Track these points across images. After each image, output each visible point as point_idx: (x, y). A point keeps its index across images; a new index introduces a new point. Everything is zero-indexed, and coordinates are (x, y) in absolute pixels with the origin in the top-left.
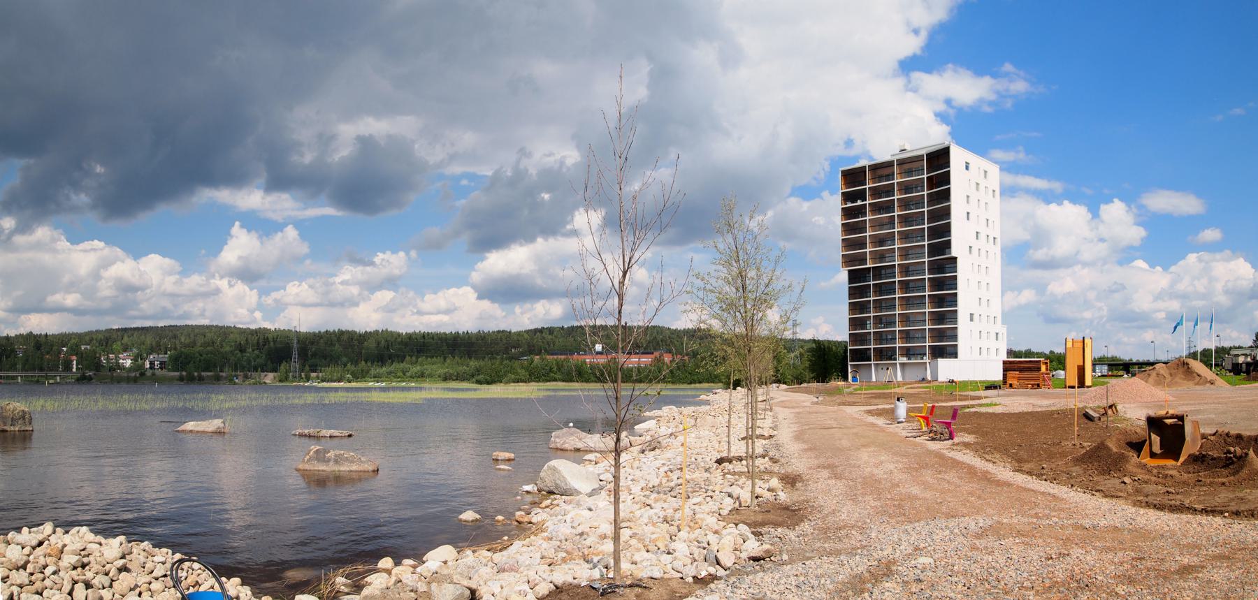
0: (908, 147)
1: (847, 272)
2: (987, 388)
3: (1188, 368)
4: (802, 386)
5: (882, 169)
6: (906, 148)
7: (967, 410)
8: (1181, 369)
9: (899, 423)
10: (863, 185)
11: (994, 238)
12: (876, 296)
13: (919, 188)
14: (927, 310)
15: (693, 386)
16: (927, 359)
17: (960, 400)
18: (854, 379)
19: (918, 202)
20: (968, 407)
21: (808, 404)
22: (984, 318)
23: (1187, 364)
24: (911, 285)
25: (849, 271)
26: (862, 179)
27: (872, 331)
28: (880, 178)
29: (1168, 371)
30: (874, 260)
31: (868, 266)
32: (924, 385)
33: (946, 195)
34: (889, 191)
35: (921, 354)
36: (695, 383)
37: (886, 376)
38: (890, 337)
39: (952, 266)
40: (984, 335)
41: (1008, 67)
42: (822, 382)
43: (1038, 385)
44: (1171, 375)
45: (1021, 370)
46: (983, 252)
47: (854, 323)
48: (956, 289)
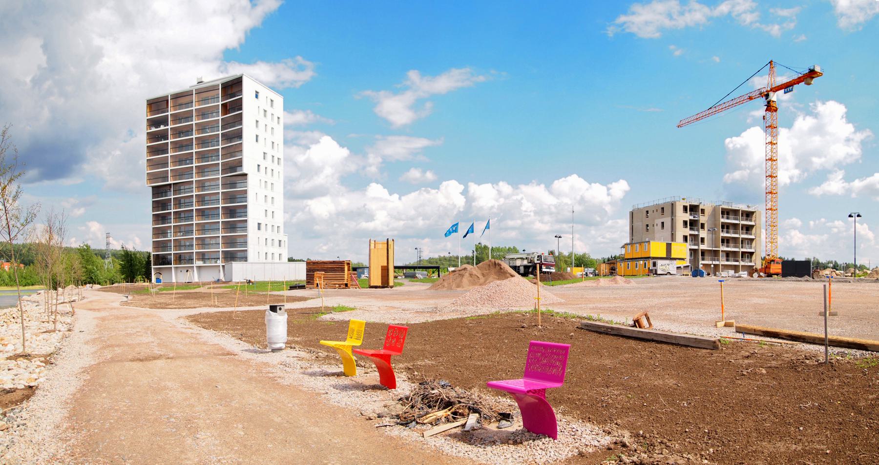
0: (205, 80)
1: (151, 188)
3: (501, 268)
4: (114, 285)
5: (180, 97)
6: (203, 80)
7: (327, 317)
8: (493, 271)
9: (274, 350)
11: (278, 159)
13: (214, 114)
14: (220, 220)
15: (26, 288)
16: (220, 263)
18: (158, 280)
19: (213, 125)
20: (329, 310)
21: (116, 304)
22: (269, 227)
23: (499, 265)
24: (207, 198)
25: (153, 187)
26: (166, 107)
27: (172, 238)
28: (180, 106)
29: (479, 271)
31: (169, 182)
32: (218, 285)
33: (239, 119)
34: (188, 116)
35: (215, 259)
36: (29, 285)
38: (188, 244)
39: (245, 181)
40: (269, 241)
42: (130, 283)
43: (346, 285)
44: (483, 275)
45: (326, 270)
46: (269, 171)
47: (157, 232)
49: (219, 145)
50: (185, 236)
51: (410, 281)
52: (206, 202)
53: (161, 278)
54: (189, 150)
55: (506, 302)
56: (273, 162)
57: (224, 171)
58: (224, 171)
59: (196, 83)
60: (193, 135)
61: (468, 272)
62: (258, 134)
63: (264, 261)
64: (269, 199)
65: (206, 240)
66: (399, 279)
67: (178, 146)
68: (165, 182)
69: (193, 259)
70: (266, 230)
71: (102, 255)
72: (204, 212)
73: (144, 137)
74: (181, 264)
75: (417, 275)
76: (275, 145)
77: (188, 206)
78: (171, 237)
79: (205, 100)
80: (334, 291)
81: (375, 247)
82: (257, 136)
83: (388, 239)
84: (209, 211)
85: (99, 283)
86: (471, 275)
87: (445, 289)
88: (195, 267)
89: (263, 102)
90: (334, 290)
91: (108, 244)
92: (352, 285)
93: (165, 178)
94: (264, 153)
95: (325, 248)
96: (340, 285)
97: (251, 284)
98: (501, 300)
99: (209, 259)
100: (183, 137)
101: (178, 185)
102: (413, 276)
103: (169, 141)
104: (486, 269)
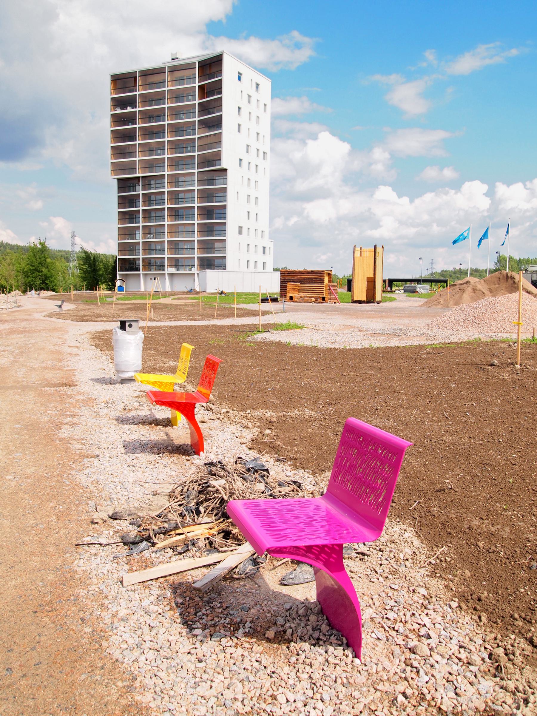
1: (116, 181)
2: (264, 300)
3: (514, 282)
6: (178, 56)
7: (259, 337)
8: (504, 285)
10: (133, 92)
11: (264, 153)
12: (145, 206)
13: (190, 97)
14: (196, 222)
16: (194, 270)
17: (239, 316)
19: (188, 111)
22: (252, 232)
23: (513, 278)
24: (181, 195)
25: (119, 180)
28: (151, 85)
29: (486, 286)
30: (143, 168)
31: (137, 175)
34: (159, 98)
35: (189, 265)
37: (153, 286)
38: (159, 247)
39: (225, 177)
40: (252, 248)
41: (295, 34)
43: (323, 299)
44: (490, 290)
45: (302, 281)
46: (253, 166)
47: (123, 233)
48: (225, 218)
49: (195, 134)
50: (156, 238)
51: (407, 296)
52: (180, 200)
53: (124, 286)
54: (160, 138)
55: (499, 325)
56: (258, 156)
57: (201, 164)
58: (200, 165)
59: (169, 59)
60: (165, 121)
61: (471, 286)
62: (240, 123)
63: (245, 269)
64: (253, 199)
65: (180, 244)
66: (396, 293)
67: (148, 133)
68: (133, 174)
69: (165, 266)
70: (248, 235)
71: (66, 257)
72: (178, 211)
73: (108, 120)
74: (151, 271)
75: (418, 290)
76: (261, 136)
77: (159, 204)
78: (140, 239)
79: (180, 80)
80: (308, 306)
81: (361, 255)
82: (239, 125)
83: (375, 246)
84: (183, 210)
85: (54, 290)
86: (474, 290)
87: (440, 307)
88: (166, 275)
89: (247, 86)
90: (309, 304)
91: (73, 244)
92: (330, 299)
93: (133, 169)
94: (248, 146)
95: (324, 257)
96: (316, 299)
97: (223, 295)
98: (492, 323)
99: (183, 265)
100: (153, 122)
101: (149, 178)
102: (414, 291)
103: (137, 126)
104: (494, 283)
